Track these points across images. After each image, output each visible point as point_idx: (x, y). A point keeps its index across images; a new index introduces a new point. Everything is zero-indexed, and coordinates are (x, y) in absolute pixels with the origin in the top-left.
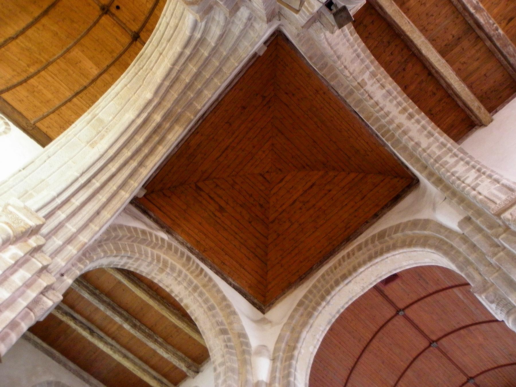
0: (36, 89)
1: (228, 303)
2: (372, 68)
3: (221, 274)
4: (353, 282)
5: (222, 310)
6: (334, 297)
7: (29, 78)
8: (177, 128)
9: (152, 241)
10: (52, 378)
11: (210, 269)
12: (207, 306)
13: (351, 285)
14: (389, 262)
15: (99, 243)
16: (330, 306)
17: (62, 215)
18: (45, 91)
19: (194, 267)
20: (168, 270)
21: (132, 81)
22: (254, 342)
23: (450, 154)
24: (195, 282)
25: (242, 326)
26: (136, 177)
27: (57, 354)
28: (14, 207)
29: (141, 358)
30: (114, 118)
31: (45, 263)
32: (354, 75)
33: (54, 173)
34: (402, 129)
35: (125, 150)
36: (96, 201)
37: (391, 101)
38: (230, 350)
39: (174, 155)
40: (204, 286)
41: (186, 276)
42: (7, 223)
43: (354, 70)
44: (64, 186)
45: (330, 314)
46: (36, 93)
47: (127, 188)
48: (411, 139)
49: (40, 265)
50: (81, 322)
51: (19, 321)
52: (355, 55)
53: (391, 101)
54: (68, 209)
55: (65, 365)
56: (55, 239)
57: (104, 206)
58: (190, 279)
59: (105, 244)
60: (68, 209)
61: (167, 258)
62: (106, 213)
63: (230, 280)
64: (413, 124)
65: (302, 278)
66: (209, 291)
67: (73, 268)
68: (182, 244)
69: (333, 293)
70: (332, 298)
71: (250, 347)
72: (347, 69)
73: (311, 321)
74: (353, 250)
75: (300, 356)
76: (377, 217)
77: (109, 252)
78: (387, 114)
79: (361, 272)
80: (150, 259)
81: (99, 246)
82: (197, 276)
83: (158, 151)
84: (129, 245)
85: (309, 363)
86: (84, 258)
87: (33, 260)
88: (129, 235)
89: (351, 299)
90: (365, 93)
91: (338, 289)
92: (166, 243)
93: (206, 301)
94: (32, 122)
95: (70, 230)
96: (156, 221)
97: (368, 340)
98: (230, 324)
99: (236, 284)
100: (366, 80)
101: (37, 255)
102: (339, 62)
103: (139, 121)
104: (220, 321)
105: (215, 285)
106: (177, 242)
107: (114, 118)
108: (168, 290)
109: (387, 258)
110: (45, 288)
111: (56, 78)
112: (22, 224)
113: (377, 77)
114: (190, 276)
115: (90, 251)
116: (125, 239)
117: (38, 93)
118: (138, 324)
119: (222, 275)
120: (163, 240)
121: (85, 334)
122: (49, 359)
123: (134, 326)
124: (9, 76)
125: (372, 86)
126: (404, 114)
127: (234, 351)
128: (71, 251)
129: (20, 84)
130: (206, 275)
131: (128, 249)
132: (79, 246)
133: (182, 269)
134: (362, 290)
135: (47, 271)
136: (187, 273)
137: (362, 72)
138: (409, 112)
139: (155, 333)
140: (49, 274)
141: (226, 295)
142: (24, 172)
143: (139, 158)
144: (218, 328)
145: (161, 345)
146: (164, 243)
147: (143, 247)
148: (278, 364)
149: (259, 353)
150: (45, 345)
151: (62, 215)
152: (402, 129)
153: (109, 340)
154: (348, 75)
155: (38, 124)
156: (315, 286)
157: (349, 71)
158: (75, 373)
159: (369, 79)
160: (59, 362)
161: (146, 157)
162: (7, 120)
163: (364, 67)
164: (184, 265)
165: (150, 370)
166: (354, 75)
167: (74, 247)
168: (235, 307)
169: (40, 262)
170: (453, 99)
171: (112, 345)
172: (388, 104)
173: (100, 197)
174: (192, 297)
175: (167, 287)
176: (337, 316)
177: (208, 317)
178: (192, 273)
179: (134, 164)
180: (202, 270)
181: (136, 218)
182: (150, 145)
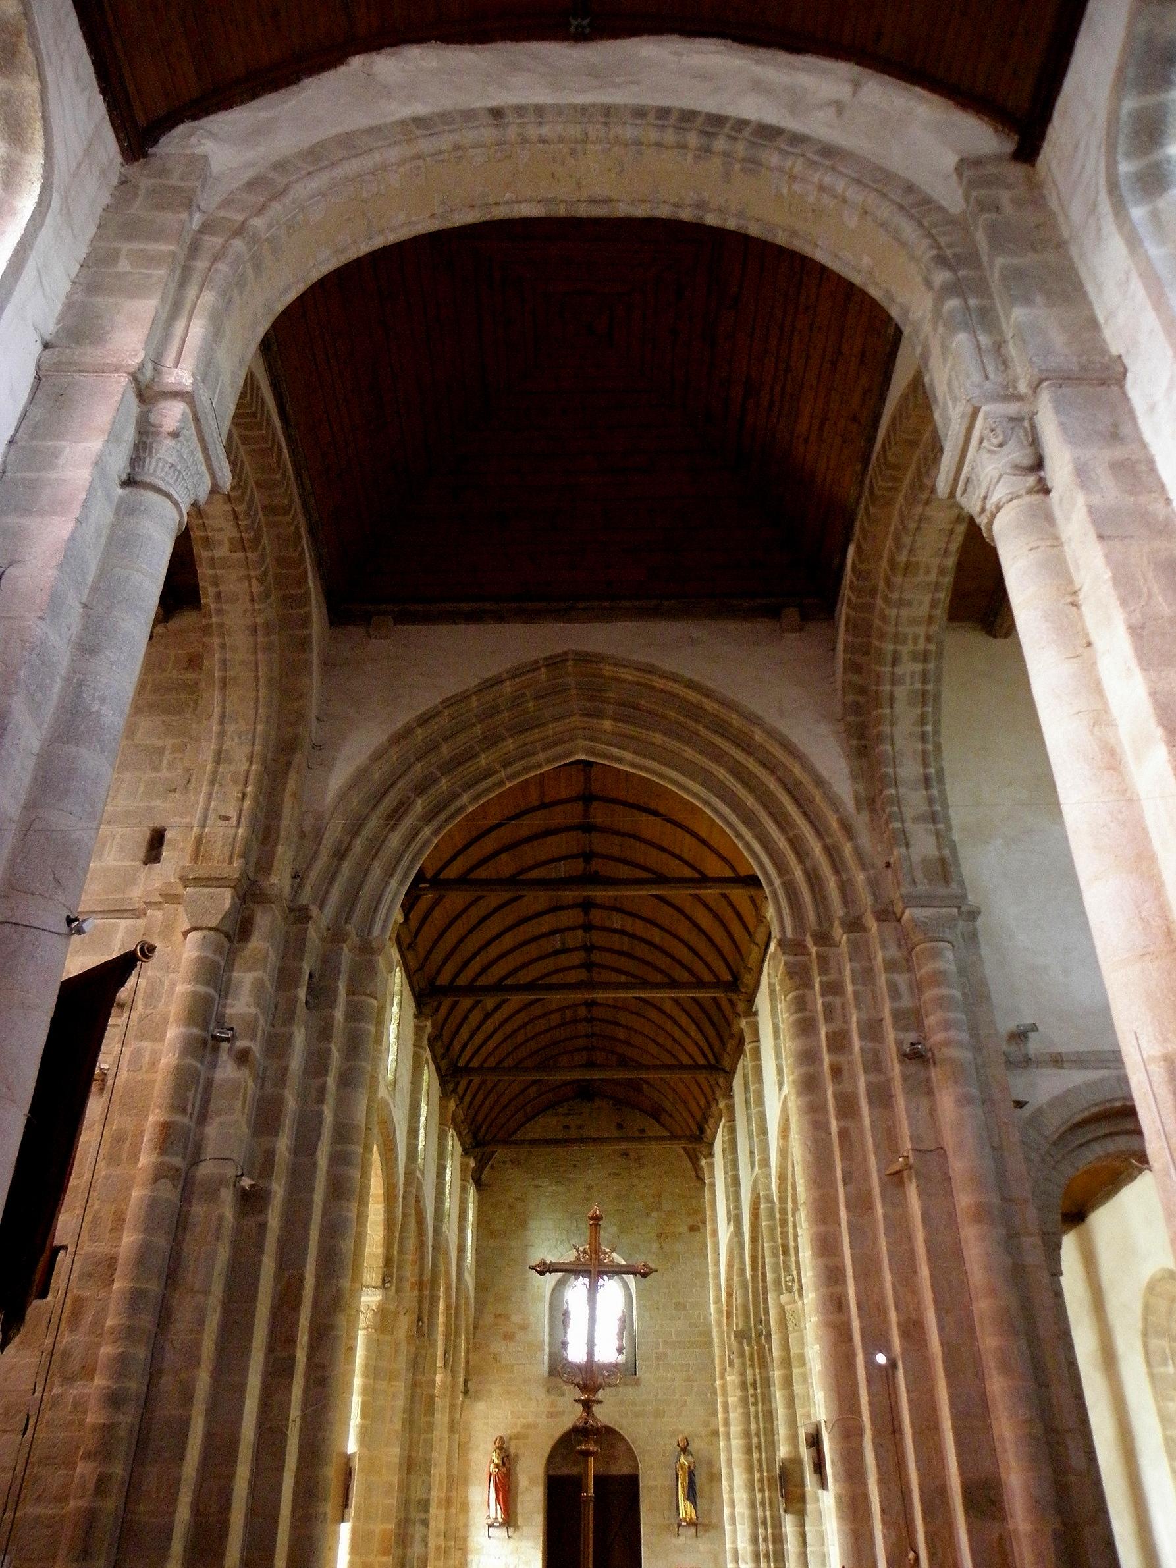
2: (206, 554)
4: (585, 195)
13: (599, 191)
32: (243, 572)
43: (239, 579)
102: (258, 620)
125: (221, 529)
148: (394, 753)
154: (254, 581)
159: (221, 543)
166: (243, 572)
170: (767, 1382)
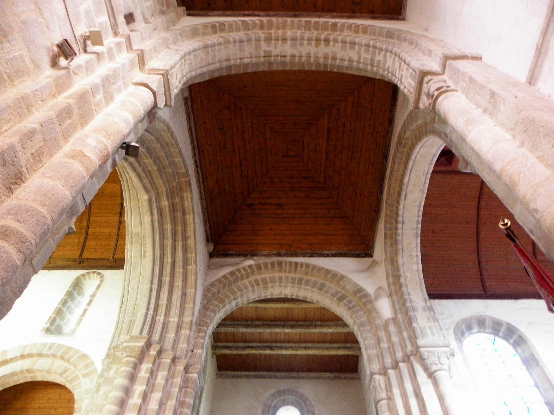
0: (96, 234)
1: (333, 273)
3: (314, 253)
4: (408, 193)
5: (331, 282)
7: (87, 231)
8: (185, 195)
9: (242, 276)
10: (272, 391)
11: (304, 256)
13: (408, 197)
14: (420, 159)
15: (205, 308)
16: (406, 224)
17: (160, 318)
18: (103, 230)
19: (288, 268)
20: (270, 285)
21: (131, 193)
22: (370, 290)
23: (377, 51)
24: (297, 276)
25: (356, 284)
26: (189, 249)
27: (265, 373)
28: (125, 342)
29: (318, 342)
30: (141, 227)
31: (171, 357)
32: (254, 55)
33: (137, 295)
34: (330, 57)
35: (166, 242)
36: (177, 289)
37: (302, 44)
38: (354, 309)
39: (207, 205)
40: (306, 274)
41: (287, 278)
42: (127, 356)
43: (250, 53)
44: (146, 301)
45: (412, 229)
46: (98, 237)
48: (342, 60)
49: (169, 361)
50: (259, 347)
51: (184, 399)
52: (237, 44)
53: (302, 44)
54: (162, 310)
55: (276, 377)
56: (169, 335)
58: (292, 278)
59: (210, 305)
60: (162, 310)
61: (263, 276)
62: (190, 290)
63: (326, 252)
64: (334, 46)
65: (377, 211)
66: (312, 275)
67: (198, 340)
68: (269, 255)
69: (401, 213)
70: (403, 216)
71: (370, 295)
72: (244, 58)
73: (400, 246)
74: (392, 167)
75: (407, 280)
76: (391, 121)
77: (216, 308)
78: (309, 56)
79: (408, 181)
80: (250, 289)
81: (207, 310)
82: (295, 271)
83: (188, 220)
84: (228, 291)
85: (420, 279)
87: (163, 360)
88: (222, 286)
89: (420, 206)
90: (276, 58)
91: (401, 207)
92: (254, 267)
93: (314, 285)
94: (111, 258)
95: (174, 321)
96: (239, 255)
97: (476, 216)
98: (344, 288)
99: (333, 252)
100: (267, 49)
101: (163, 356)
103: (156, 217)
104: (334, 292)
105: (314, 267)
106: (263, 258)
107: (141, 227)
109: (416, 157)
110: (185, 369)
111: (101, 215)
112: (137, 349)
113: (273, 38)
114: (290, 275)
116: (221, 290)
117: (99, 235)
118: (294, 323)
119: (317, 254)
120: (250, 266)
121: (268, 352)
122: (262, 380)
123: (292, 327)
124: (77, 241)
125: (276, 48)
126: (320, 44)
127: (358, 308)
129: (86, 239)
130: (302, 265)
131: (229, 294)
133: (281, 274)
134: (423, 193)
135: (178, 359)
136: (287, 274)
137: (258, 47)
138: (322, 39)
139: (311, 321)
142: (123, 306)
143: (180, 237)
144: (335, 299)
145: (322, 326)
146: (253, 269)
147: (240, 283)
148: (394, 297)
149: (377, 297)
150: (252, 373)
152: (330, 57)
153: (287, 345)
155: (116, 257)
156: (386, 215)
157: (247, 58)
158: (285, 378)
159: (269, 46)
160: (270, 377)
161: (184, 231)
162: (98, 271)
163: (255, 43)
164: (280, 271)
165: (332, 345)
166: (254, 55)
167: (186, 329)
168: (341, 272)
171: (292, 347)
172: (301, 49)
173: (177, 284)
174: (302, 290)
175: (280, 295)
176: (420, 226)
177: (323, 295)
178: (290, 272)
179: (180, 244)
180: (296, 263)
181: (222, 266)
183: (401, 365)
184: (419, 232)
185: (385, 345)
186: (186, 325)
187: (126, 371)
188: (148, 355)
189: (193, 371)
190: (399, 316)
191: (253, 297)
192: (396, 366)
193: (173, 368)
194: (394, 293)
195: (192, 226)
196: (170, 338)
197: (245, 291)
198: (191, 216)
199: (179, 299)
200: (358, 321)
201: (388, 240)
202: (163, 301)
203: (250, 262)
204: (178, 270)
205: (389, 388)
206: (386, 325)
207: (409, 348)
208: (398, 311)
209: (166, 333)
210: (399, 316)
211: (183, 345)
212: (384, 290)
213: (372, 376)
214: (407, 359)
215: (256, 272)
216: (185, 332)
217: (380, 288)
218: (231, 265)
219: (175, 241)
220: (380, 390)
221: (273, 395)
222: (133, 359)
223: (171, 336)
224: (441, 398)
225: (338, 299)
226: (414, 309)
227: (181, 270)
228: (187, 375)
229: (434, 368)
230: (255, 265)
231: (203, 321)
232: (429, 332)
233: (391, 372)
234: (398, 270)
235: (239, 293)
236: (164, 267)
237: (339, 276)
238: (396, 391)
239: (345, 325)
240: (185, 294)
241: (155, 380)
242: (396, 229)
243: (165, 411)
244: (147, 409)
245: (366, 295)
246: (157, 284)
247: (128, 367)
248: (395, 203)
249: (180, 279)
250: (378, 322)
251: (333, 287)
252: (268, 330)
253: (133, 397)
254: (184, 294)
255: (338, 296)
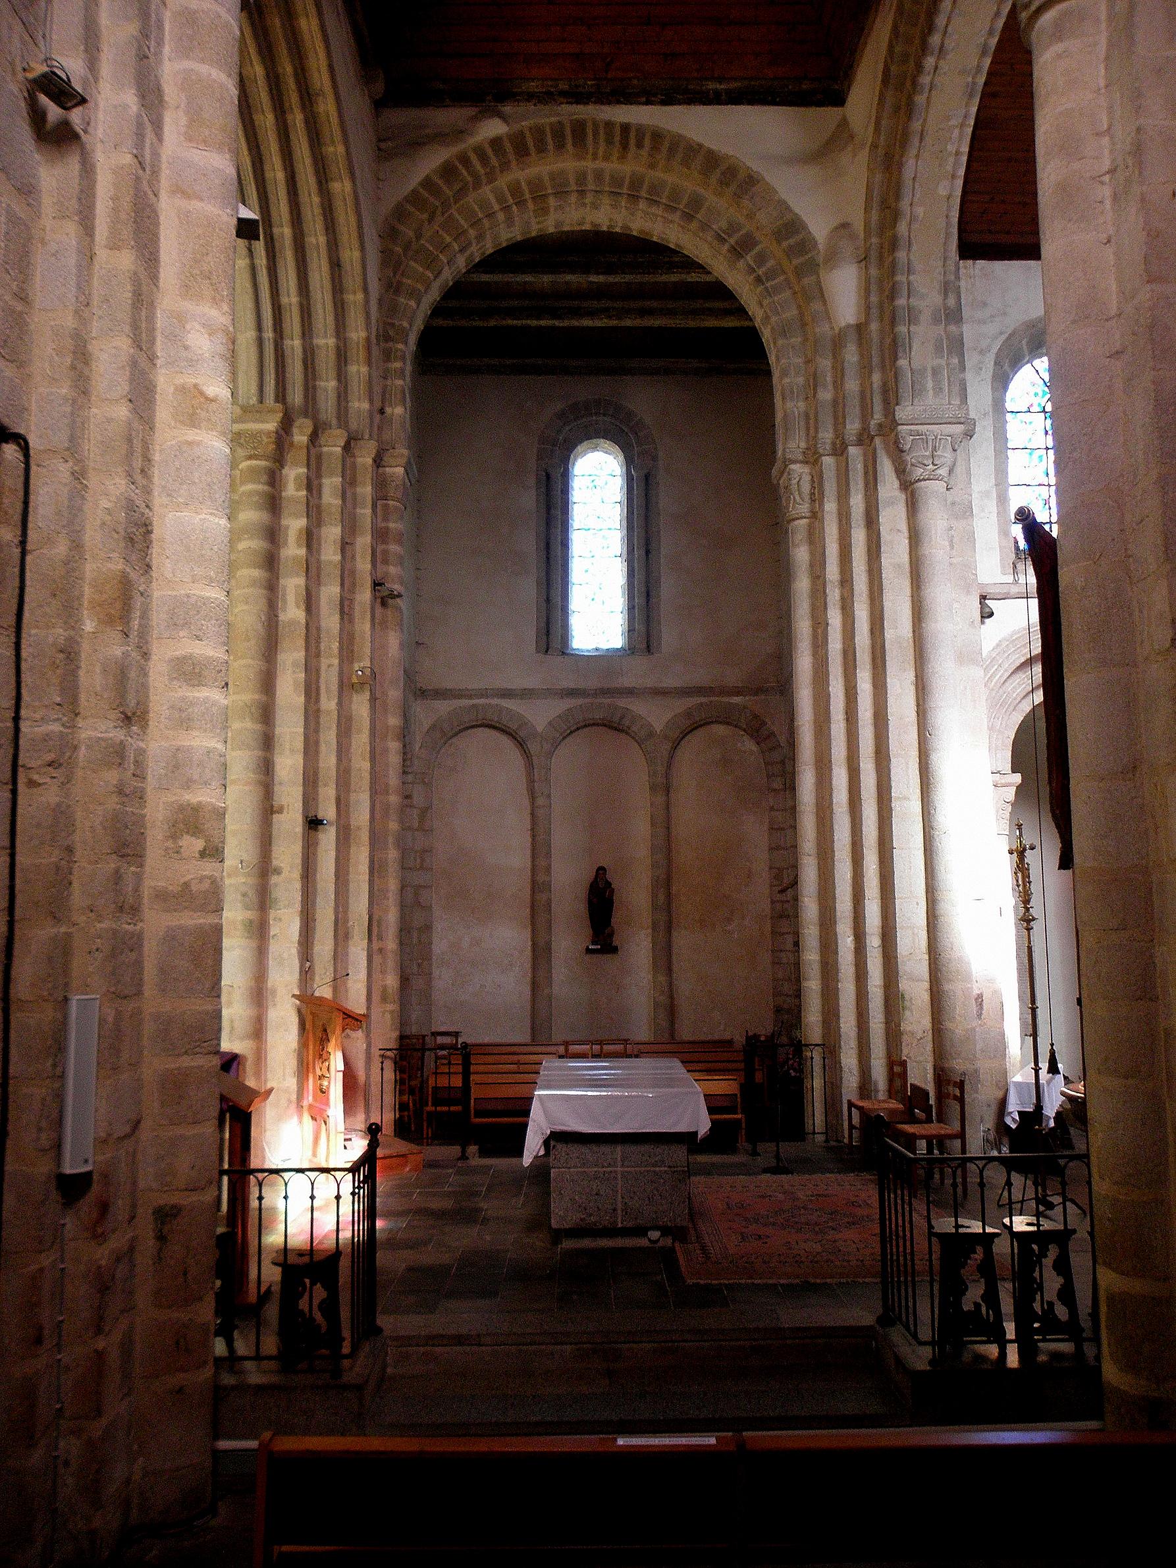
6: (950, 29)
10: (560, 406)
12: (679, 213)
15: (392, 287)
17: (294, 344)
22: (819, 228)
24: (627, 168)
35: (258, 118)
40: (652, 166)
42: (250, 458)
47: (334, 168)
56: (322, 384)
57: (333, 245)
67: (389, 382)
69: (940, 21)
73: (916, 125)
75: (915, 226)
80: (501, 216)
81: (397, 291)
85: (948, 224)
86: (391, 344)
87: (325, 449)
88: (425, 216)
98: (750, 216)
108: (587, 227)
110: (375, 461)
114: (612, 166)
115: (390, 321)
120: (496, 142)
123: (609, 270)
128: (358, 371)
132: (362, 354)
140: (362, 442)
141: (714, 147)
143: (293, 97)
147: (471, 199)
148: (874, 272)
149: (832, 257)
151: (294, 344)
153: (595, 304)
164: (580, 158)
169: (335, 446)
176: (988, 61)
178: (606, 158)
179: (297, 119)
182: (282, 51)
183: (853, 450)
184: (981, 80)
185: (826, 395)
186: (357, 354)
187: (258, 493)
188: (292, 444)
189: (392, 461)
190: (874, 326)
191: (510, 235)
192: (839, 450)
193: (349, 461)
194: (874, 254)
195: (322, 54)
196: (326, 390)
197: (486, 223)
198: (315, 22)
199: (327, 284)
200: (774, 319)
201: (889, 94)
202: (290, 298)
203: (494, 128)
204: (307, 199)
205: (817, 497)
206: (837, 343)
207: (878, 417)
208: (875, 311)
209: (314, 379)
210: (874, 326)
211: (360, 405)
212: (853, 237)
213: (786, 466)
214: (864, 439)
215: (514, 163)
216: (358, 370)
217: (845, 226)
218: (442, 137)
219: (283, 112)
220: (797, 498)
221: (561, 415)
222: (263, 463)
223: (328, 385)
224: (915, 538)
225: (733, 250)
226: (913, 317)
227: (316, 200)
228: (381, 470)
229: (919, 472)
230: (509, 136)
231: (393, 325)
232: (930, 384)
233: (828, 461)
234: (898, 197)
235: (472, 233)
236: (271, 196)
237: (742, 175)
238: (830, 506)
239: (741, 312)
240: (339, 266)
241: (320, 497)
242: (919, 68)
243: (353, 557)
244: (318, 561)
245: (805, 245)
246: (263, 253)
247: (259, 482)
248: (908, 84)
249: (319, 225)
250: (823, 329)
251: (721, 207)
252: (547, 279)
253: (286, 543)
254: (336, 265)
255: (732, 241)
